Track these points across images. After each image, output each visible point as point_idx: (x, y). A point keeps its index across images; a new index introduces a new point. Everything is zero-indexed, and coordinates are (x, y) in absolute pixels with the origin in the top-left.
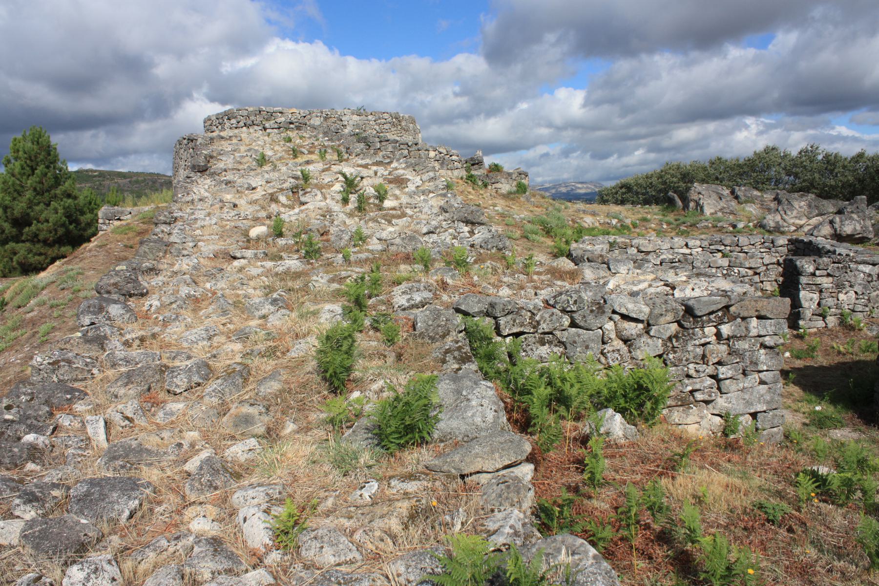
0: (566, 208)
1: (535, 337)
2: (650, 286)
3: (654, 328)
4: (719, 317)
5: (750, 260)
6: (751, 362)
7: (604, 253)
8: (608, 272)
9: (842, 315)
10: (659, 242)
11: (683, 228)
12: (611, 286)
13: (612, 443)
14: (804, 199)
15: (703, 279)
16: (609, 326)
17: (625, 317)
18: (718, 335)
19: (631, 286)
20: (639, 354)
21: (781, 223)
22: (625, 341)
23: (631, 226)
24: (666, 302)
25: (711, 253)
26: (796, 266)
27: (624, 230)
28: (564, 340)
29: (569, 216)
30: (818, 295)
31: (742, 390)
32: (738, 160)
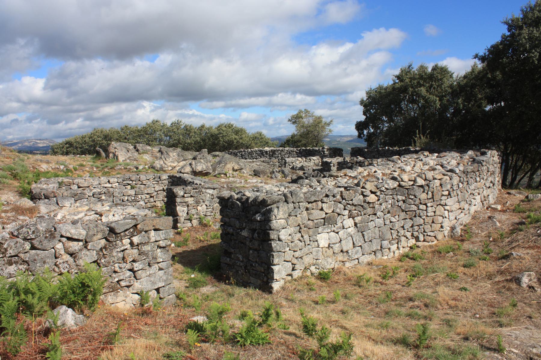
0: (28, 159)
1: (4, 260)
2: (86, 215)
3: (90, 244)
4: (131, 232)
6: (153, 258)
7: (55, 190)
8: (58, 206)
9: (200, 218)
10: (92, 180)
11: (106, 170)
12: (59, 217)
13: (67, 330)
14: (175, 151)
15: (120, 208)
16: (59, 246)
17: (69, 239)
18: (132, 244)
19: (73, 216)
20: (81, 262)
21: (163, 165)
22: (71, 255)
23: (73, 170)
24: (97, 226)
25: (124, 186)
26: (173, 192)
27: (68, 172)
28: (27, 259)
29: (30, 164)
30: (187, 208)
31: (149, 276)
32: (137, 127)
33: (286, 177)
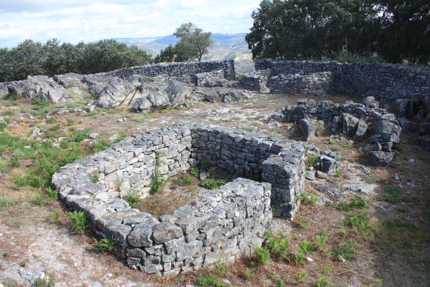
5: (172, 152)
33: (238, 100)
